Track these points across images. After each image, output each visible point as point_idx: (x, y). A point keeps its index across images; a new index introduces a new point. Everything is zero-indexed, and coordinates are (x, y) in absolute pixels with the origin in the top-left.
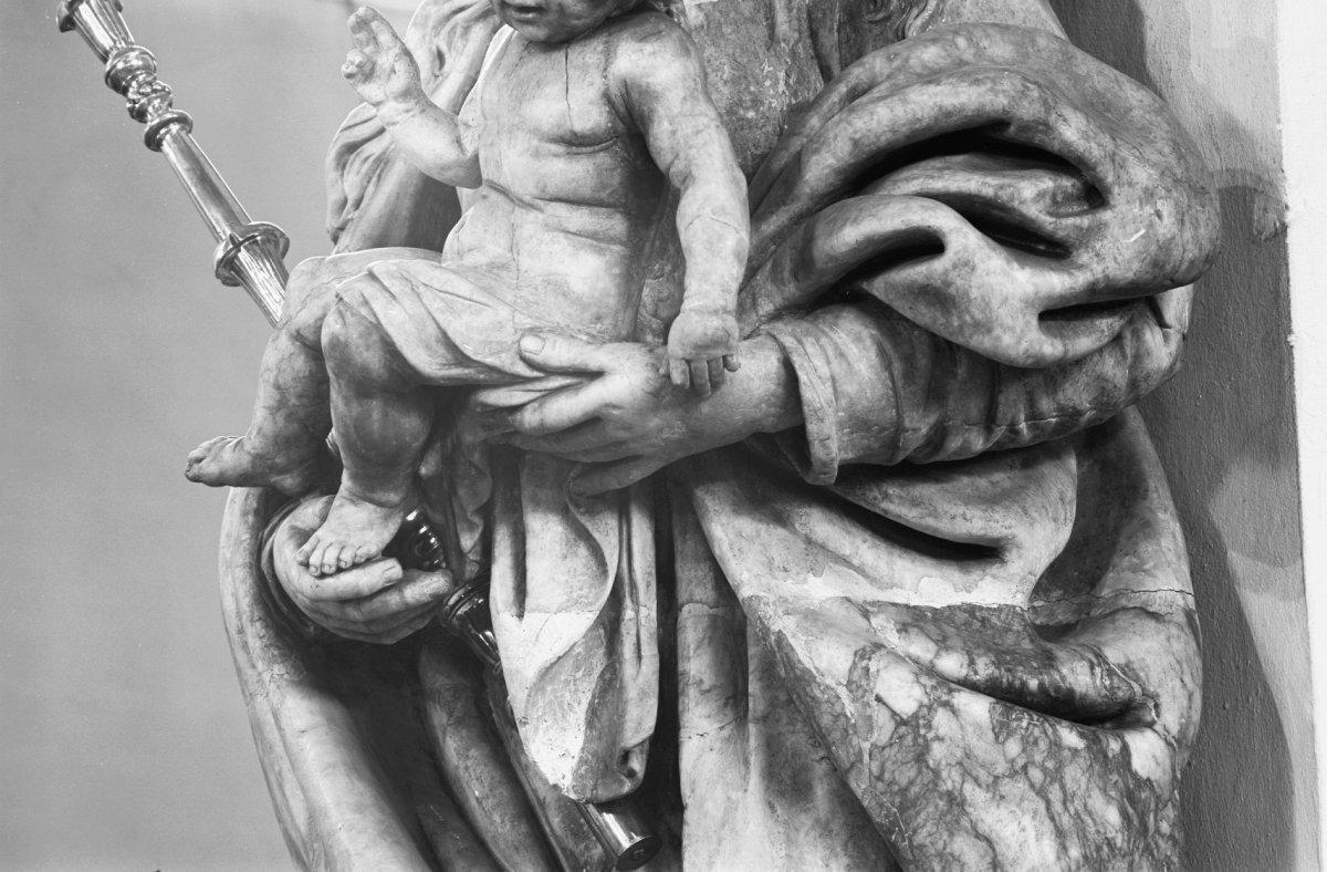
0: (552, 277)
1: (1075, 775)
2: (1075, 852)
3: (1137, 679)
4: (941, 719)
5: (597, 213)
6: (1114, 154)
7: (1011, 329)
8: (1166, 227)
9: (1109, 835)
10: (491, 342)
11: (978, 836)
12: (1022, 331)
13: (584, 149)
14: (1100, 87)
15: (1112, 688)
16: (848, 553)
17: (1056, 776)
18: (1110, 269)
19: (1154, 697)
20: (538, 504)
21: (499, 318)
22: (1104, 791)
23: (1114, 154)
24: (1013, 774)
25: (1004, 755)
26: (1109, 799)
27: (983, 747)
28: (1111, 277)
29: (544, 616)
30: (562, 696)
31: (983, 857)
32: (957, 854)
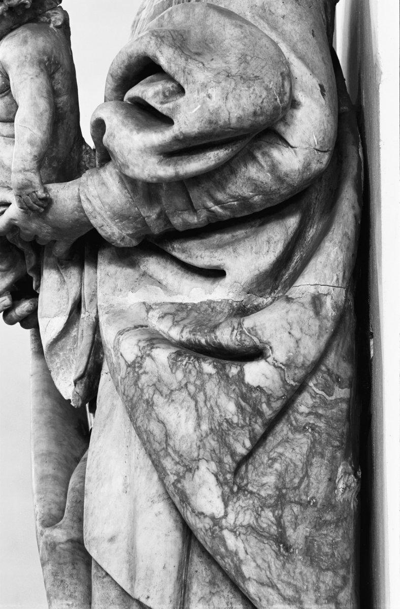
1: (211, 387)
2: (205, 427)
3: (256, 335)
4: (148, 363)
7: (137, 165)
8: (215, 101)
9: (228, 417)
11: (159, 421)
12: (143, 165)
15: (241, 340)
16: (162, 278)
17: (202, 388)
19: (268, 343)
22: (227, 394)
23: (185, 68)
24: (180, 389)
25: (176, 379)
26: (230, 398)
27: (166, 375)
28: (184, 133)
29: (48, 319)
30: (69, 357)
31: (161, 432)
32: (151, 430)
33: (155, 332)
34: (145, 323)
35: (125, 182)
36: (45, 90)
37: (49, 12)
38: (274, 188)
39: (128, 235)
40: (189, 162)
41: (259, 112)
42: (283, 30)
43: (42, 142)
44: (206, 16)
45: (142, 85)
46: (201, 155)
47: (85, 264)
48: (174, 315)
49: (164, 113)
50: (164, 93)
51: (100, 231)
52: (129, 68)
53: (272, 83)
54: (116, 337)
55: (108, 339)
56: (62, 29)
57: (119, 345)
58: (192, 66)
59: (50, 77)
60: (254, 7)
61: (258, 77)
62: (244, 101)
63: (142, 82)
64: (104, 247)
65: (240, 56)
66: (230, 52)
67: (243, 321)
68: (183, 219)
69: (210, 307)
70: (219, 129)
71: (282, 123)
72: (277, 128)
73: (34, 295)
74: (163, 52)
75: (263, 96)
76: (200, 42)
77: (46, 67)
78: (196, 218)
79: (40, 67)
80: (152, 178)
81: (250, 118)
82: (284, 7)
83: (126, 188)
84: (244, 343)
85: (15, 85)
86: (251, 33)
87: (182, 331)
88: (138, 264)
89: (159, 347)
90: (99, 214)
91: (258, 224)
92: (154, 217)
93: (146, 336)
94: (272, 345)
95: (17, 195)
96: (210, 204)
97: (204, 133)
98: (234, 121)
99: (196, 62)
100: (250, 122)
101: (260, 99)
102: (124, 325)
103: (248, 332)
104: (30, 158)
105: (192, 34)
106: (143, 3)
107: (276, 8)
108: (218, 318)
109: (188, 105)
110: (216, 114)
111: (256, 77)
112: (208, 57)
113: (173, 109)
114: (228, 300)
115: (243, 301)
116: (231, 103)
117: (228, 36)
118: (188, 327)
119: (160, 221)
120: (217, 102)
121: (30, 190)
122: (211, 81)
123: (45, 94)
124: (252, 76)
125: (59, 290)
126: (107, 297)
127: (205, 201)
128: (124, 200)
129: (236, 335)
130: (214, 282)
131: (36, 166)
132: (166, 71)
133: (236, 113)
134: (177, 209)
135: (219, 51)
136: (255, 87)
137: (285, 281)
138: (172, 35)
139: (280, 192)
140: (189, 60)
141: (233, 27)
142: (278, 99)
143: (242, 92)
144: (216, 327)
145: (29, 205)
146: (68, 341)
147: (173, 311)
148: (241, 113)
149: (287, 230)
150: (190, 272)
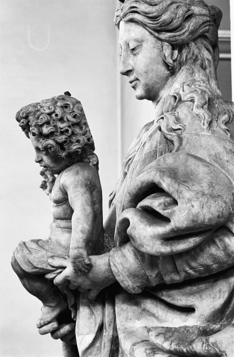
0: (57, 241)
3: (217, 347)
5: (68, 222)
6: (178, 190)
7: (149, 245)
8: (196, 209)
10: (41, 261)
12: (152, 246)
13: (60, 204)
14: (192, 168)
16: (155, 312)
18: (177, 225)
19: (224, 352)
20: (108, 303)
21: (43, 254)
28: (177, 227)
29: (83, 336)
33: (154, 344)
34: (147, 339)
35: (138, 255)
36: (89, 201)
37: (90, 156)
38: (225, 260)
39: (137, 286)
40: (179, 244)
41: (221, 216)
42: (228, 169)
43: (88, 231)
44: (187, 160)
45: (149, 199)
46: (186, 240)
47: (106, 303)
48: (164, 334)
49: (165, 215)
50: (164, 204)
51: (121, 284)
52: (140, 189)
53: (228, 199)
54: (131, 347)
55: (126, 348)
56: (96, 166)
57: (133, 352)
58: (183, 188)
59: (91, 193)
60: (210, 156)
61: (220, 195)
62: (213, 209)
63: (148, 197)
64: (119, 293)
65: (209, 183)
66: (203, 181)
67: (209, 338)
68: (171, 277)
69: (185, 329)
70: (198, 225)
71: (231, 222)
72: (228, 225)
73: (72, 322)
74: (164, 180)
75: (223, 207)
76: (185, 175)
77: (89, 188)
78: (178, 277)
79: (86, 188)
80: (157, 253)
81: (216, 219)
82: (227, 156)
83: (138, 259)
84: (210, 352)
85: (72, 198)
86: (214, 170)
87: (171, 344)
88: (140, 303)
89: (159, 354)
90: (121, 274)
91: (212, 281)
92: (154, 276)
93: (149, 347)
94: (227, 353)
95: (73, 262)
96: (187, 269)
97: (189, 227)
98: (206, 220)
99: (185, 186)
100: (215, 222)
101: (221, 208)
102: (135, 340)
103: (212, 345)
104: (81, 240)
105: (180, 170)
106: (130, 152)
107: (223, 156)
108: (191, 337)
109: (180, 211)
110: (197, 216)
111: (219, 195)
112: (191, 184)
113: (171, 213)
114: (197, 326)
115: (205, 326)
116: (205, 210)
117: (201, 172)
118: (174, 342)
119: (157, 278)
120: (197, 210)
121: (81, 259)
122: (193, 197)
123: (90, 204)
124: (216, 195)
125: (89, 318)
126: (123, 323)
127: (185, 267)
128: (136, 265)
129: (205, 347)
130: (187, 315)
131: (85, 245)
132: (167, 191)
133: (208, 216)
134: (167, 272)
135: (197, 180)
136: (219, 201)
137: (227, 315)
138: (168, 171)
139: (228, 263)
140: (181, 185)
141: (203, 167)
142: (231, 209)
143: (211, 204)
144: (192, 342)
145: (80, 268)
146: (94, 350)
147: (163, 332)
148: (211, 216)
149: (230, 285)
150: (172, 309)
